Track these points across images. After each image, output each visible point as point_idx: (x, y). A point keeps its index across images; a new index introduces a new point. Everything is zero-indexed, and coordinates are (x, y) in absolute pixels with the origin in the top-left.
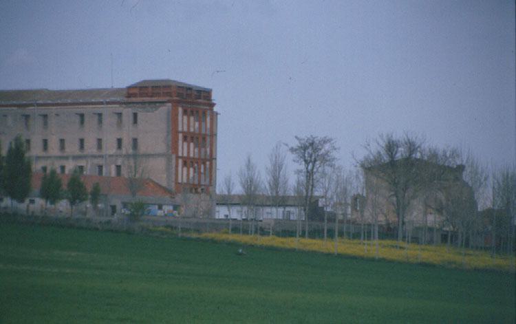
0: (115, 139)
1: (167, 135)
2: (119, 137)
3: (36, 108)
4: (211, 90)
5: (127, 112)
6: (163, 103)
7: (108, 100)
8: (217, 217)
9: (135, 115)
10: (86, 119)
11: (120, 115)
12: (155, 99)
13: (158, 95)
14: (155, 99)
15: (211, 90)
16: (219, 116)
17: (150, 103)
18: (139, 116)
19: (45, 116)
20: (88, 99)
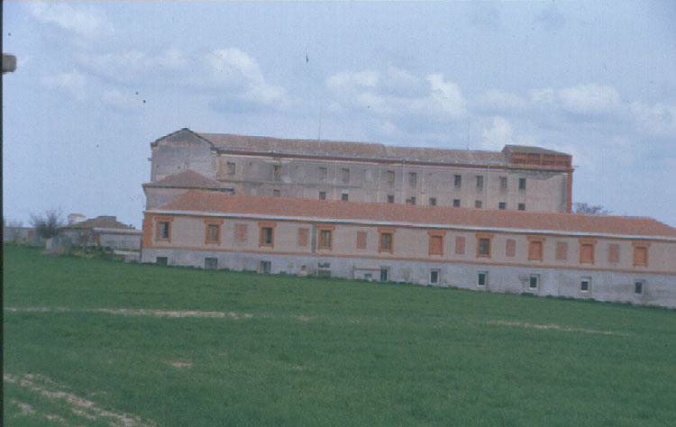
0: (474, 201)
1: (562, 204)
2: (502, 201)
3: (404, 165)
4: (571, 156)
5: (513, 179)
6: (559, 172)
7: (407, 160)
8: (141, 228)
9: (522, 182)
10: (463, 181)
11: (504, 179)
12: (548, 167)
13: (552, 163)
14: (548, 167)
15: (571, 156)
16: (150, 156)
17: (541, 171)
18: (529, 182)
19: (413, 174)
20: (290, 152)
